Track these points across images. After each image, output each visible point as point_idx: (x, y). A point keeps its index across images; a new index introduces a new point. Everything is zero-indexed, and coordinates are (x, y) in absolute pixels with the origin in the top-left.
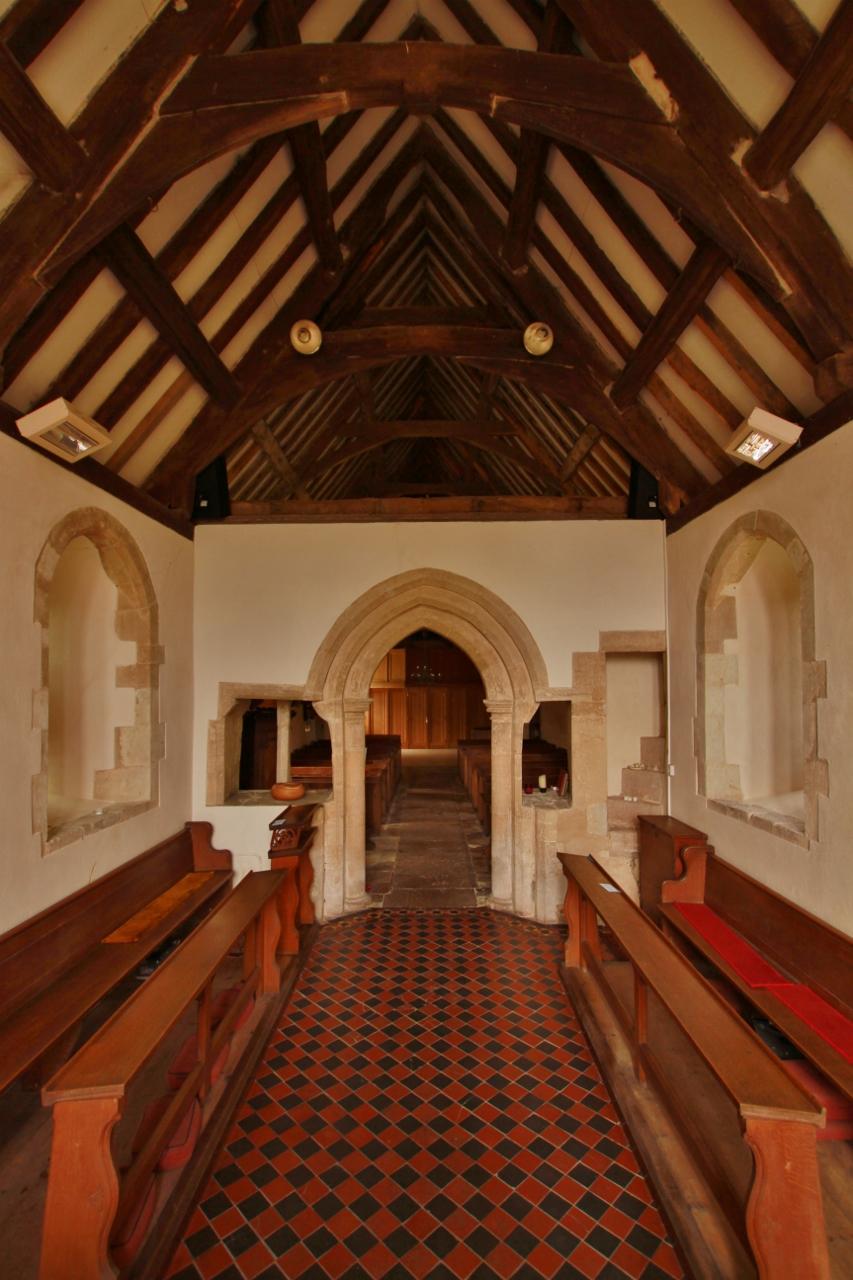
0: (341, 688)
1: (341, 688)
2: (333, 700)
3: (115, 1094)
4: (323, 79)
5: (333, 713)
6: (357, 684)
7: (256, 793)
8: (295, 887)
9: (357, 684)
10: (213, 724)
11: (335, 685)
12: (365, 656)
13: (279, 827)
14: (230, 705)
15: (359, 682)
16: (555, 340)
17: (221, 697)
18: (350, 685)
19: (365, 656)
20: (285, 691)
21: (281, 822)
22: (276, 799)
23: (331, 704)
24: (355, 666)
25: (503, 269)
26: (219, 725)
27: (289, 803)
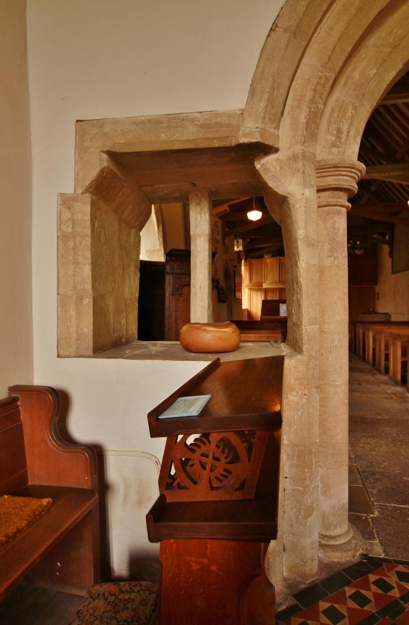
0: (311, 133)
1: (311, 133)
2: (298, 149)
3: (191, 325)
4: (390, 508)
5: (300, 175)
6: (339, 130)
7: (157, 346)
8: (266, 340)
9: (339, 130)
10: (66, 201)
11: (303, 119)
12: (356, 75)
13: (186, 424)
14: (98, 163)
15: (345, 127)
16: (4, 495)
17: (81, 149)
18: (325, 134)
19: (356, 75)
20: (205, 126)
21: (193, 406)
22: (192, 351)
23: (295, 158)
24: (336, 95)
25: (192, 430)
26: (78, 206)
27: (214, 357)
